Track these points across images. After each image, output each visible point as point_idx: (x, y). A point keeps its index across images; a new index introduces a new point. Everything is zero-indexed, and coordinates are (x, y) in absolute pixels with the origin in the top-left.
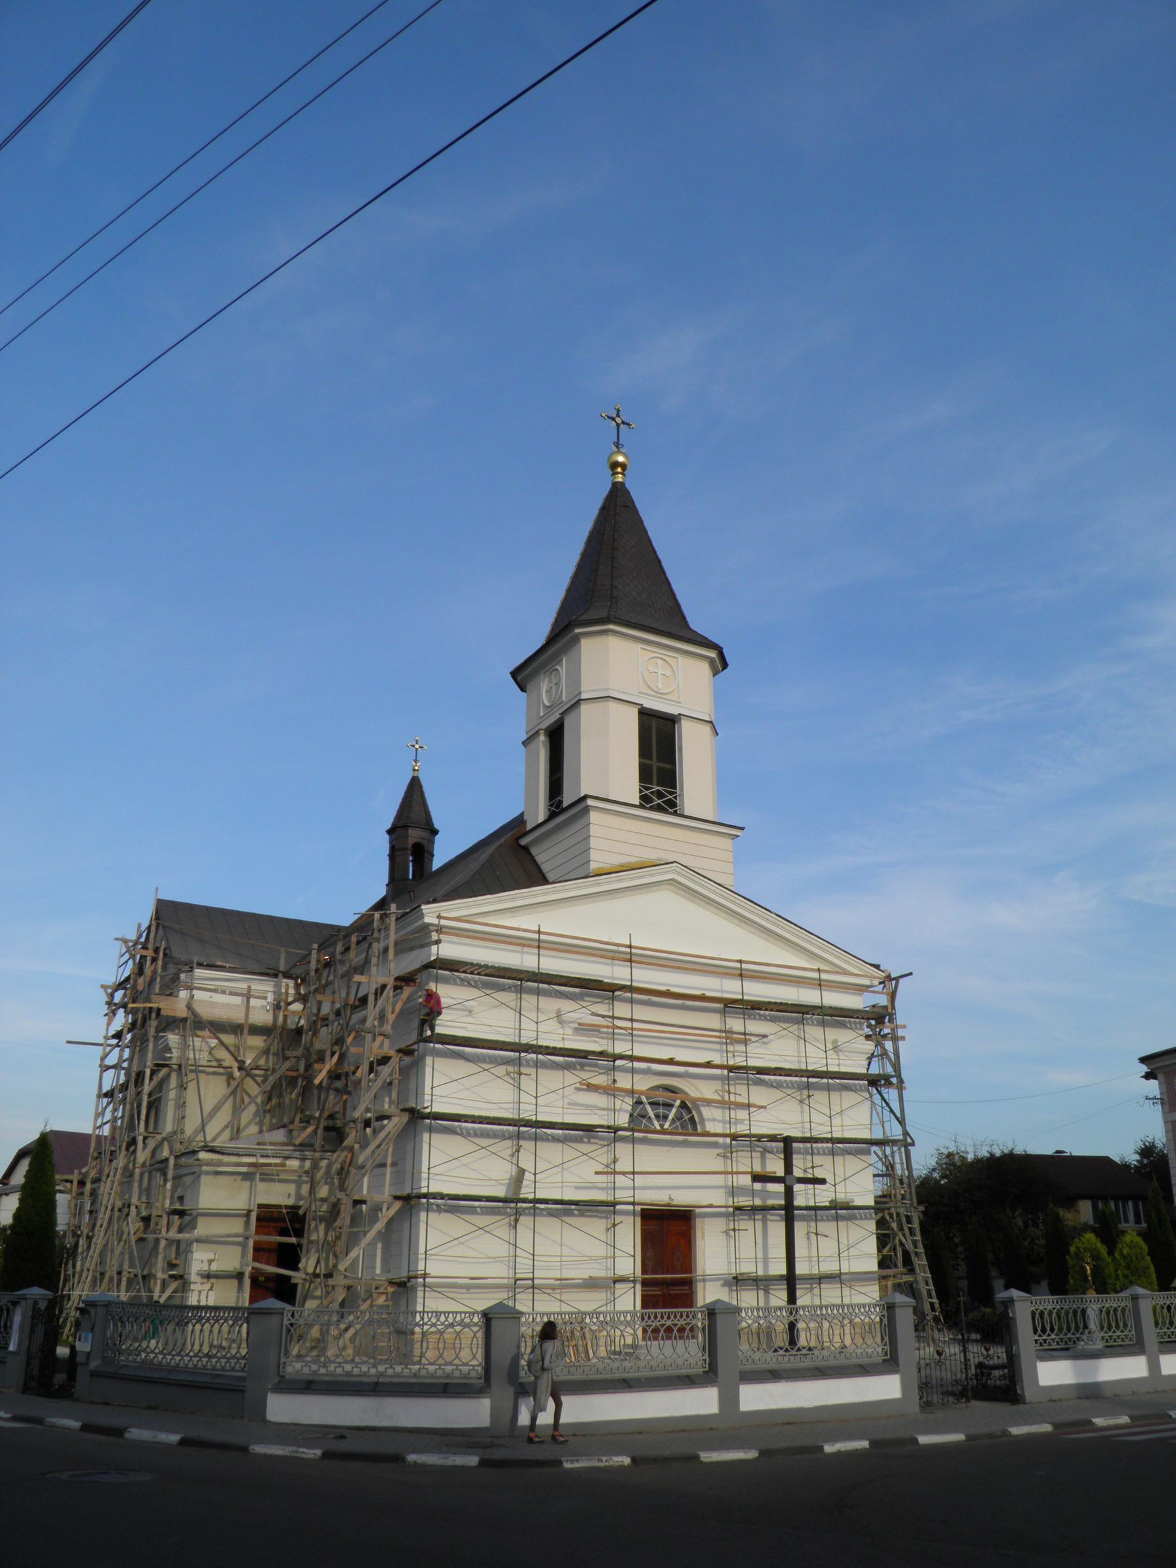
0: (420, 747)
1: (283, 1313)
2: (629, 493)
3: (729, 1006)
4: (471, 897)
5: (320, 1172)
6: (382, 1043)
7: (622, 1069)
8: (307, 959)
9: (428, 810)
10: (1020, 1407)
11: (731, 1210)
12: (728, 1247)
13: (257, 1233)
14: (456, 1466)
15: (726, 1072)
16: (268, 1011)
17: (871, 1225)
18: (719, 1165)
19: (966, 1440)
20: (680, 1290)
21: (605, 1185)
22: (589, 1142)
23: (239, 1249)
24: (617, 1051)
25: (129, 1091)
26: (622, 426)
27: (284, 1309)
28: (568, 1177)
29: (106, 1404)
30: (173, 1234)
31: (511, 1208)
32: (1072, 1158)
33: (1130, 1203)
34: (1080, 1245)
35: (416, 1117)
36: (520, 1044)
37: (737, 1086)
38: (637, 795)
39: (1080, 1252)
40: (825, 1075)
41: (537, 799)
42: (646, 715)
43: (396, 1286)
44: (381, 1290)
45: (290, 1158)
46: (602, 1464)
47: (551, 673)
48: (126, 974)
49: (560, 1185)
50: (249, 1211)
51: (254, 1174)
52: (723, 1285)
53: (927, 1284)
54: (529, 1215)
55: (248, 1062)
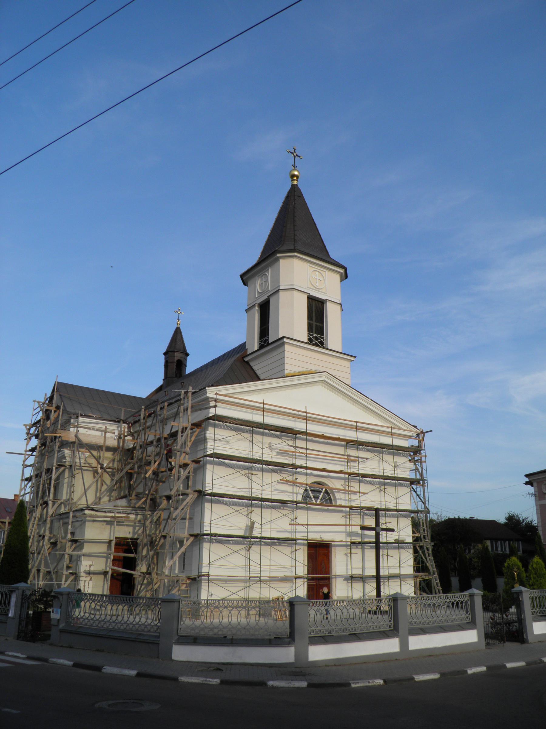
0: (181, 313)
1: (179, 602)
2: (300, 190)
3: (350, 443)
4: (230, 385)
5: (148, 521)
6: (185, 457)
7: (300, 473)
8: (139, 413)
9: (184, 344)
10: (525, 645)
11: (349, 543)
12: (347, 561)
13: (115, 551)
14: (295, 687)
15: (347, 476)
16: (115, 439)
17: (411, 551)
18: (342, 521)
19: (526, 665)
20: (324, 582)
21: (291, 530)
22: (283, 509)
23: (104, 560)
24: (297, 464)
25: (42, 478)
26: (296, 157)
27: (180, 599)
28: (274, 526)
29: (71, 647)
30: (70, 552)
31: (246, 541)
32: (478, 521)
33: (499, 542)
34: (510, 563)
35: (201, 494)
36: (252, 459)
37: (352, 483)
38: (307, 338)
39: (510, 566)
40: (394, 479)
41: (254, 338)
42: (311, 299)
43: (191, 580)
44: (184, 582)
45: (130, 514)
46: (370, 684)
47: (262, 276)
48: (38, 419)
49: (270, 530)
50: (110, 542)
51: (113, 522)
52: (344, 580)
53: (436, 580)
54: (258, 545)
55: (105, 465)
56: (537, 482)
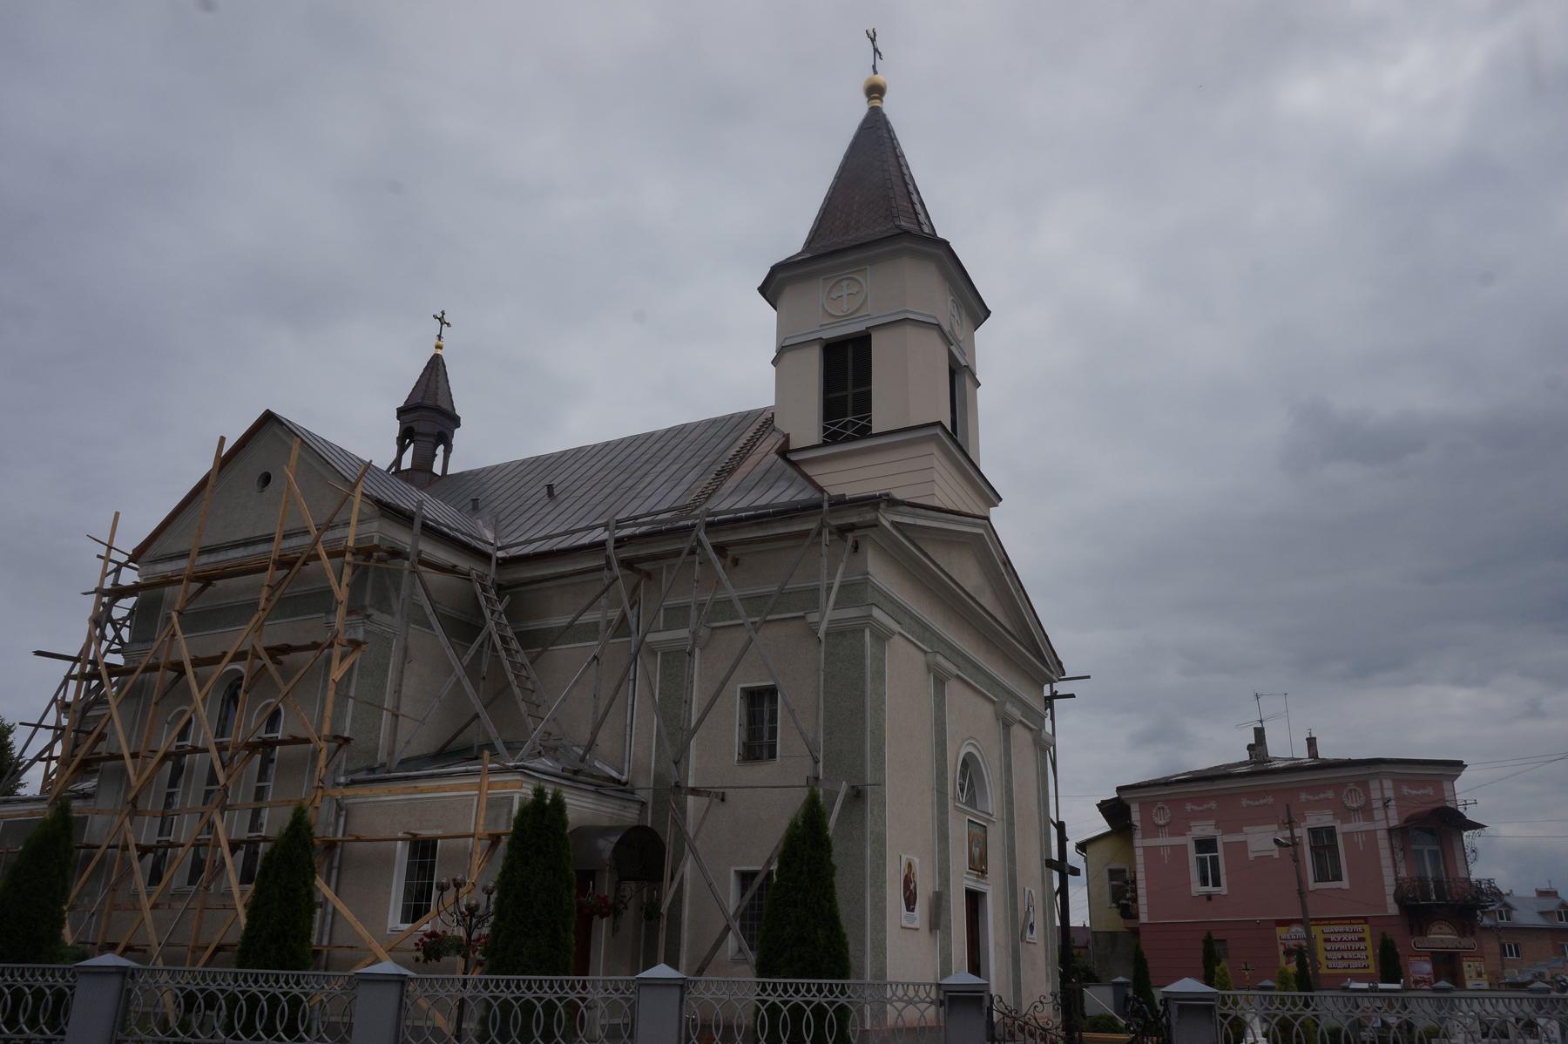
56: (1141, 805)
